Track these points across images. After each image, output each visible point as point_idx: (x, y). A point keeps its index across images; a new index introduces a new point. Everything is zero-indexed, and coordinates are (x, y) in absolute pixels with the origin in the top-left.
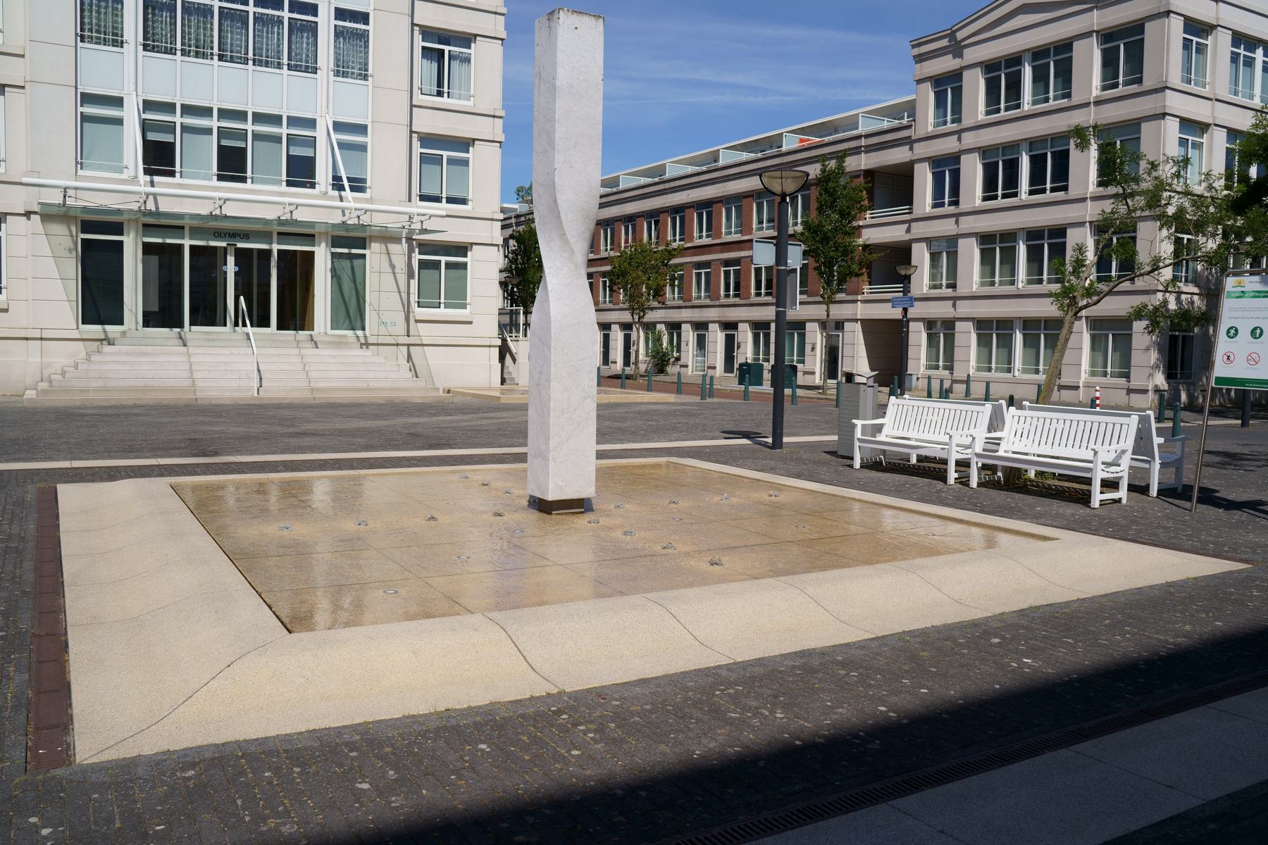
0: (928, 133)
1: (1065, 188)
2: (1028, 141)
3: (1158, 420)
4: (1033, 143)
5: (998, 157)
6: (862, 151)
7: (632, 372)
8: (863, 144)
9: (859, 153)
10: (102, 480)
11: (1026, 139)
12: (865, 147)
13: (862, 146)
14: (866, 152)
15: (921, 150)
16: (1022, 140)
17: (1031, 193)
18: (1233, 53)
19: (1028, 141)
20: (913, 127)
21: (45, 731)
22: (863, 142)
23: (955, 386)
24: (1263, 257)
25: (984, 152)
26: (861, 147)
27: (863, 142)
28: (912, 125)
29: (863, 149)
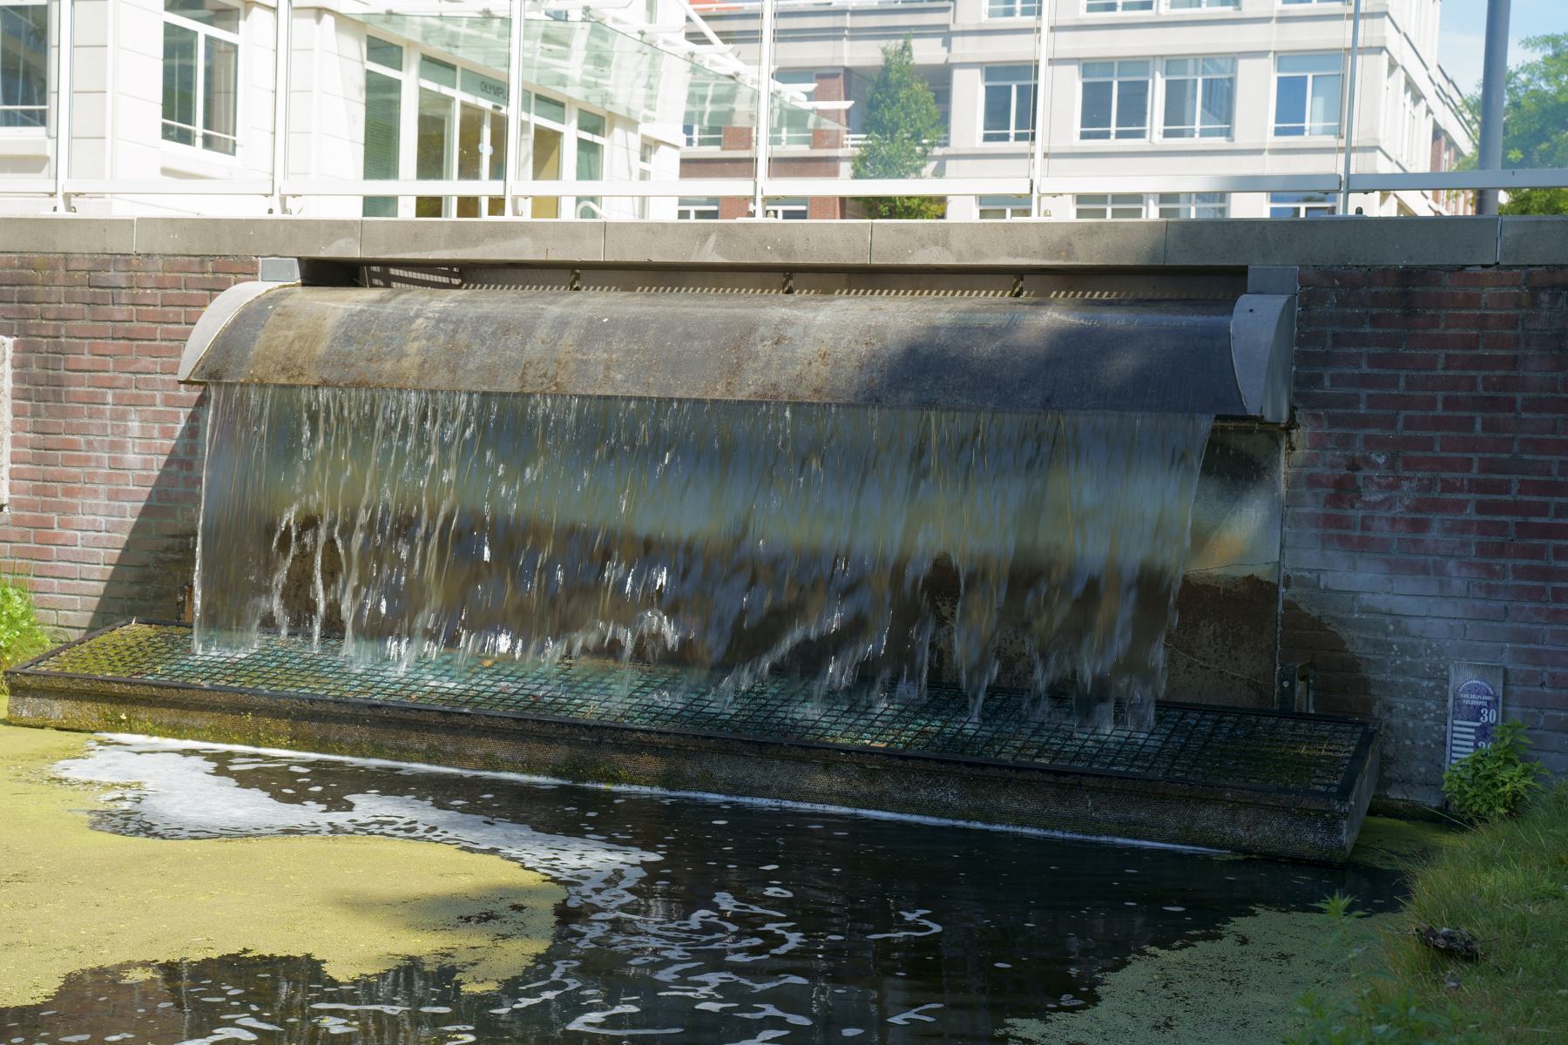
0: (980, 24)
1: (1228, 133)
2: (1165, 59)
3: (1470, 480)
4: (1172, 63)
5: (1112, 75)
6: (845, 36)
7: (1344, 145)
8: (848, 25)
9: (840, 38)
10: (440, 288)
11: (1162, 56)
12: (852, 30)
13: (847, 28)
14: (852, 38)
15: (964, 49)
16: (1155, 57)
17: (1167, 134)
18: (170, 29)
19: (1165, 59)
20: (952, 10)
21: (466, 710)
22: (849, 21)
23: (1535, 194)
24: (450, 1007)
25: (992, 71)
26: (844, 29)
27: (849, 21)
28: (950, 8)
29: (846, 32)
